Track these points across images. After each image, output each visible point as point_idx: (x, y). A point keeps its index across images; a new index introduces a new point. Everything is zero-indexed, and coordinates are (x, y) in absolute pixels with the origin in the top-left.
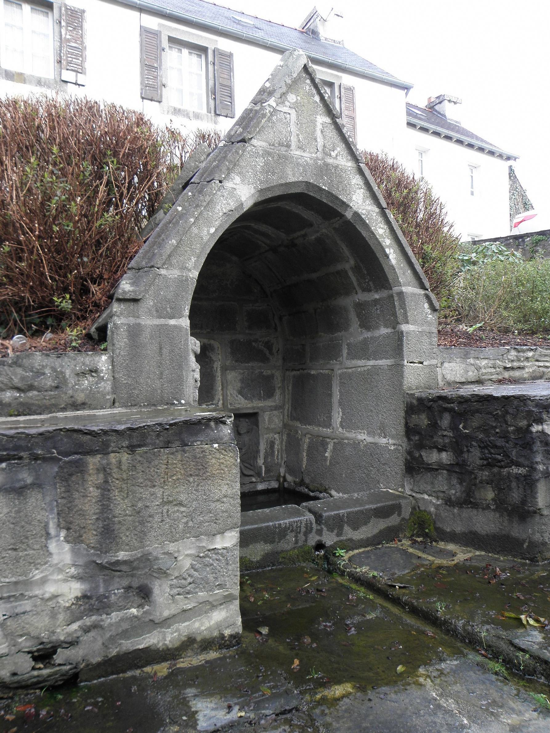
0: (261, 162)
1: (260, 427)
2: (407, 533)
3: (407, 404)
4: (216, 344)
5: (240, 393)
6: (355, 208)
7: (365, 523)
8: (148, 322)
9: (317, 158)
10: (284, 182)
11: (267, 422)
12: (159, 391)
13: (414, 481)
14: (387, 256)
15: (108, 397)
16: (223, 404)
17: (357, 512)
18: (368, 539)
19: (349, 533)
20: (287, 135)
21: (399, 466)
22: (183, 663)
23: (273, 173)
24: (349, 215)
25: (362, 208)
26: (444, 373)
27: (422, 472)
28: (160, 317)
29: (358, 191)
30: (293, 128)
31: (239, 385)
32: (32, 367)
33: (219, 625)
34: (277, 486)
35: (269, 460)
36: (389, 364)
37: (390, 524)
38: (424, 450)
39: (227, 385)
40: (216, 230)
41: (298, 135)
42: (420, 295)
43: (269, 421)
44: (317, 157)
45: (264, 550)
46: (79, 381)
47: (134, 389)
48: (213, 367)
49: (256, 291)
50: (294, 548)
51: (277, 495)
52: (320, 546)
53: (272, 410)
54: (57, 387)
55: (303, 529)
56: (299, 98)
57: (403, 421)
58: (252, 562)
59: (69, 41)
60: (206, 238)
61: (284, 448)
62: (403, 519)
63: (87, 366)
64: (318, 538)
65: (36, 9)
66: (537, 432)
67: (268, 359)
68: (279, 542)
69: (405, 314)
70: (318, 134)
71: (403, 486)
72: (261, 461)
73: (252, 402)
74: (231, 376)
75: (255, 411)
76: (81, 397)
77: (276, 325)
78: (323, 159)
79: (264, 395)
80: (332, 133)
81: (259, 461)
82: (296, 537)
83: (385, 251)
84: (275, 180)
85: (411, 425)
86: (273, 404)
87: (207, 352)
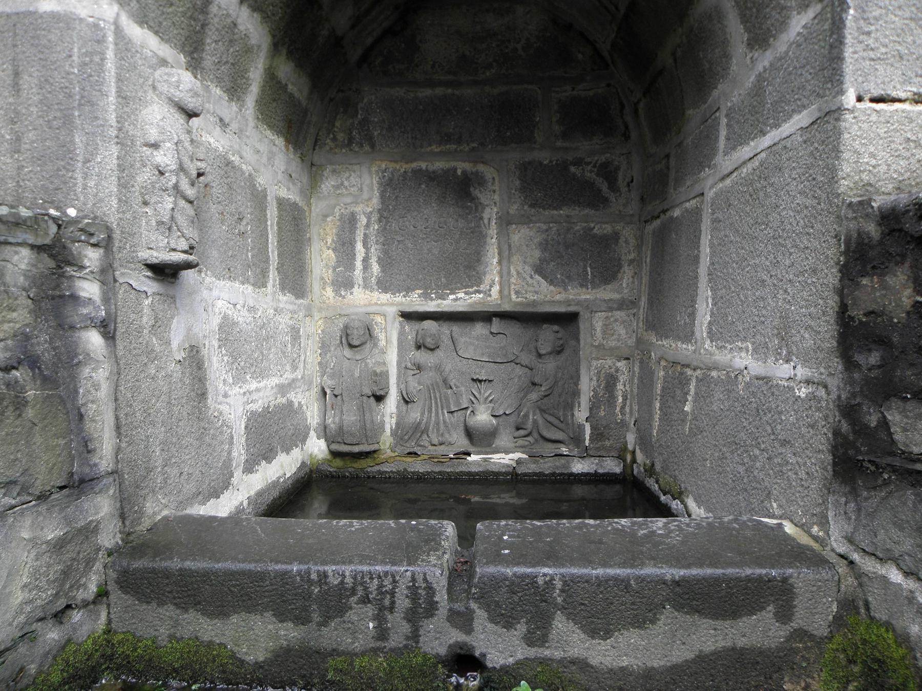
1: (582, 342)
3: (848, 243)
4: (488, 172)
5: (539, 270)
7: (639, 622)
12: (11, 184)
13: (859, 510)
16: (501, 292)
17: (601, 582)
21: (811, 458)
27: (886, 483)
31: (537, 254)
34: (618, 470)
35: (602, 413)
36: (805, 123)
37: (741, 642)
38: (895, 403)
43: (604, 332)
45: (278, 637)
48: (481, 218)
49: (580, 56)
50: (375, 651)
51: (618, 487)
53: (611, 309)
55: (403, 603)
57: (833, 302)
58: (242, 662)
61: (635, 391)
62: (801, 634)
64: (457, 636)
67: (606, 201)
68: (324, 624)
71: (824, 523)
72: (581, 414)
73: (566, 290)
74: (519, 235)
75: (572, 309)
77: (627, 127)
79: (594, 276)
81: (576, 413)
82: (379, 618)
85: (857, 313)
86: (616, 296)
87: (472, 189)
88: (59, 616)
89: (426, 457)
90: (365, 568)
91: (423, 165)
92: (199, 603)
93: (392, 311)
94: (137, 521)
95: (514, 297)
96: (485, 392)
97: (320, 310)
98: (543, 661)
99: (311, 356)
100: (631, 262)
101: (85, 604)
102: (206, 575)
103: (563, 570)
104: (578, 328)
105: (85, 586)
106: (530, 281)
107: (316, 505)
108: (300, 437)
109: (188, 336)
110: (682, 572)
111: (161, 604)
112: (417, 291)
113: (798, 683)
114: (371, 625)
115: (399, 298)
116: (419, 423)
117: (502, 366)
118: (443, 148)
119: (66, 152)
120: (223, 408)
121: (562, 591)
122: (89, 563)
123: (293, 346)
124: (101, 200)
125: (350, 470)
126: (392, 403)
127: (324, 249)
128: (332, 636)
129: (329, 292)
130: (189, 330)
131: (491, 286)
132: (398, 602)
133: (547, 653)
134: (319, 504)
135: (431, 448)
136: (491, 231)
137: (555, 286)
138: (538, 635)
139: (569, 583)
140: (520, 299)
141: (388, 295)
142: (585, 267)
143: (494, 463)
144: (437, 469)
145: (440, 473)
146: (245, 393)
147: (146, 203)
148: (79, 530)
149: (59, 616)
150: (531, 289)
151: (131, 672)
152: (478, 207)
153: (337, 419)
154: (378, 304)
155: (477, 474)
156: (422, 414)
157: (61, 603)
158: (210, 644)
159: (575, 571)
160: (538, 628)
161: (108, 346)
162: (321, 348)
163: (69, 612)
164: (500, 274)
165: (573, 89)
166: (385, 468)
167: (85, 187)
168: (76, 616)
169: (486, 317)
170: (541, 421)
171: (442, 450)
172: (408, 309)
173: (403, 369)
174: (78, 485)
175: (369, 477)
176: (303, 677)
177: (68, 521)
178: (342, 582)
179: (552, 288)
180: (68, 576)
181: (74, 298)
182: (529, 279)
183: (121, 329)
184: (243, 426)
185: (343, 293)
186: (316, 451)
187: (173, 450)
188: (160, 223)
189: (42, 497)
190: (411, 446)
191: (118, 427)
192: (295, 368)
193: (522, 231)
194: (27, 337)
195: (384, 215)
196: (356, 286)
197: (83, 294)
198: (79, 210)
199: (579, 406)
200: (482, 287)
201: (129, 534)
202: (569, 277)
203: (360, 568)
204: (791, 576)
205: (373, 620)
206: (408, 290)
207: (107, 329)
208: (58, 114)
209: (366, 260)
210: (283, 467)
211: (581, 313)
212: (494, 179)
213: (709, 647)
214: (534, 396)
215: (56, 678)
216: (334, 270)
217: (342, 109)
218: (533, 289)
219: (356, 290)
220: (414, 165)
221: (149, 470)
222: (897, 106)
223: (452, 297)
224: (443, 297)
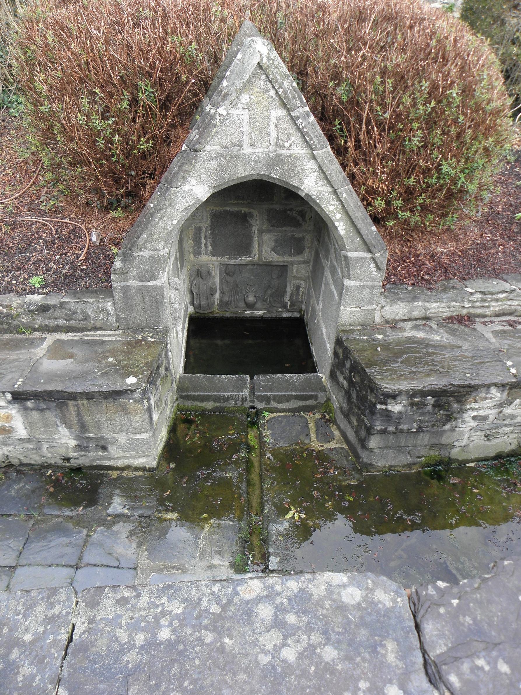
0: (214, 164)
4: (255, 212)
5: (273, 250)
7: (288, 401)
8: (134, 284)
11: (295, 272)
14: (336, 228)
16: (259, 257)
17: (280, 396)
19: (273, 404)
20: (240, 135)
22: (125, 474)
23: (226, 172)
24: (303, 195)
25: (314, 189)
28: (141, 281)
29: (311, 175)
30: (246, 128)
31: (273, 244)
33: (142, 463)
39: (262, 244)
41: (250, 134)
43: (297, 271)
44: (269, 152)
53: (299, 264)
54: (85, 319)
55: (240, 399)
56: (252, 97)
60: (170, 228)
64: (251, 404)
66: (380, 409)
69: (349, 272)
70: (272, 128)
72: (287, 299)
74: (266, 237)
76: (98, 325)
80: (287, 125)
82: (236, 402)
86: (302, 259)
91: (228, 209)
97: (188, 262)
100: (308, 248)
115: (219, 259)
118: (236, 202)
126: (217, 296)
128: (226, 404)
129: (192, 256)
152: (250, 226)
164: (258, 251)
171: (236, 310)
173: (221, 282)
195: (213, 227)
206: (223, 256)
219: (202, 255)
220: (224, 208)
224: (237, 259)
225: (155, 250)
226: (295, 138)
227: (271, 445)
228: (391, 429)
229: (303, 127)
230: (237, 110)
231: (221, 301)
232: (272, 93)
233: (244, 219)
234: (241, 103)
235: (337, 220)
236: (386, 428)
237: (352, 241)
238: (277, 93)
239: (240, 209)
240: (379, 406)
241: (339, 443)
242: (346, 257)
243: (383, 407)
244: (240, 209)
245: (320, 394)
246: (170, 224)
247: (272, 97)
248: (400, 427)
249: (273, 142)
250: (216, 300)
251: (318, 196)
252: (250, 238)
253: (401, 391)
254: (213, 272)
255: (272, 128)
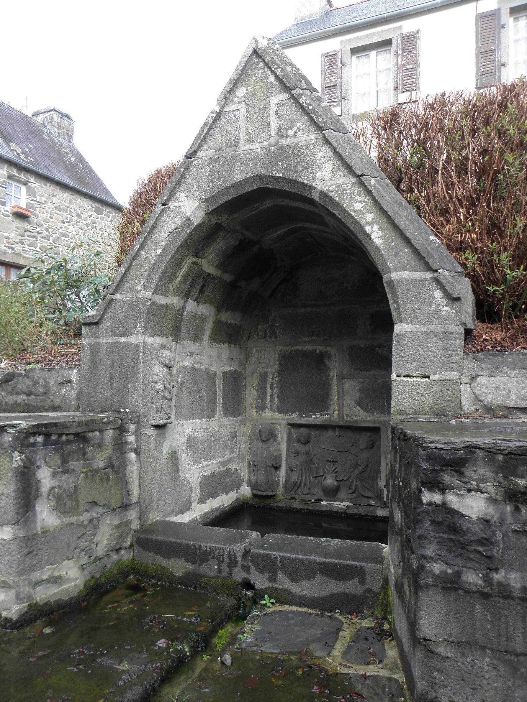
0: (206, 171)
2: (376, 613)
4: (333, 351)
5: (359, 403)
6: (319, 188)
8: (105, 340)
9: (270, 145)
10: (229, 184)
14: (368, 236)
15: (73, 403)
16: (339, 415)
17: (294, 560)
18: (313, 599)
19: (284, 582)
24: (316, 197)
25: (329, 184)
26: (477, 392)
28: (114, 336)
29: (325, 165)
30: (242, 124)
31: (358, 395)
32: (34, 378)
37: (347, 591)
40: (163, 250)
41: (247, 129)
42: (424, 280)
46: (60, 389)
47: (92, 397)
48: (329, 375)
50: (218, 577)
52: (248, 585)
54: (45, 393)
55: (226, 560)
58: (174, 575)
59: (404, 65)
62: (369, 590)
63: (64, 377)
64: (244, 575)
65: (381, 52)
66: (430, 504)
68: (200, 565)
70: (273, 116)
72: (382, 484)
73: (373, 414)
74: (349, 385)
75: (376, 425)
76: (57, 402)
78: (276, 143)
80: (290, 110)
82: (219, 565)
83: (364, 231)
84: (220, 185)
88: (118, 551)
89: (300, 500)
90: (214, 545)
91: (300, 348)
92: (161, 552)
93: (284, 422)
94: (146, 521)
95: (345, 417)
96: (333, 467)
97: (250, 421)
98: (275, 589)
99: (244, 445)
101: (126, 548)
102: (163, 542)
103: (281, 554)
104: (380, 436)
105: (126, 542)
106: (354, 409)
107: (246, 520)
108: (238, 485)
109: (170, 448)
110: (324, 560)
111: (150, 551)
112: (297, 413)
113: (369, 611)
114: (216, 567)
115: (288, 416)
116: (297, 482)
117: (342, 454)
119: (126, 388)
120: (188, 476)
121: (280, 562)
122: (128, 534)
123: (231, 441)
124: (137, 405)
125: (263, 504)
126: (283, 472)
127: (252, 390)
128: (203, 570)
129: (254, 412)
130: (172, 445)
131: (334, 412)
132: (225, 559)
133: (276, 585)
134: (247, 521)
135: (302, 496)
136: (334, 383)
137: (367, 412)
138: (273, 579)
139: (283, 559)
140: (348, 419)
141: (282, 414)
142: (384, 402)
143: (335, 507)
144: (306, 507)
145: (307, 509)
146: (200, 468)
147: (153, 403)
148: (125, 522)
149: (118, 551)
150: (355, 414)
151: (140, 575)
152: (328, 369)
153: (256, 477)
154: (276, 418)
155: (326, 511)
156: (298, 478)
157: (118, 547)
158: (164, 568)
159: (285, 554)
160: (273, 575)
161: (137, 457)
162: (250, 440)
163: (120, 550)
164: (338, 405)
165: (377, 307)
166: (280, 505)
167: (132, 401)
168: (123, 552)
169: (334, 427)
170: (360, 486)
171: (308, 497)
172: (292, 422)
174: (125, 507)
175: (272, 508)
176: (194, 584)
177: (121, 519)
178: (206, 550)
179: (366, 413)
180: (121, 537)
181: (126, 443)
182: (353, 408)
183: (142, 450)
184: (198, 483)
185: (261, 413)
186: (246, 493)
187: (162, 494)
188: (157, 410)
189: (113, 510)
190: (292, 494)
191: (140, 486)
192: (232, 452)
193: (350, 382)
194: (111, 458)
195: (281, 373)
196: (267, 410)
197: (129, 441)
198: (129, 410)
199: (381, 479)
200: (329, 412)
201: (142, 525)
202: (375, 408)
203: (212, 545)
204: (364, 566)
205: (217, 565)
206: (292, 412)
207: (137, 452)
208: (124, 376)
209: (272, 396)
210: (224, 500)
211: (381, 428)
212: (335, 355)
213: (335, 591)
214: (357, 472)
215: (116, 571)
216: (257, 401)
217: (261, 320)
218: (355, 414)
219: (266, 411)
220: (296, 348)
221: (151, 502)
222: (415, 379)
223: (314, 416)
224: (309, 416)
225: (135, 291)
226: (301, 122)
227: (244, 645)
228: (472, 578)
229: (308, 105)
230: (233, 106)
231: (287, 482)
232: (272, 78)
233: (319, 361)
234: (238, 97)
235: (368, 224)
236: (458, 574)
237: (396, 255)
238: (277, 77)
239: (315, 347)
240: (427, 497)
241: (390, 669)
242: (391, 282)
243: (437, 498)
244: (315, 347)
245: (368, 566)
246: (153, 255)
247: (271, 83)
248: (497, 577)
249: (273, 133)
250: (281, 479)
251: (336, 192)
252: (326, 386)
253: (471, 448)
254: (279, 435)
255: (273, 116)
